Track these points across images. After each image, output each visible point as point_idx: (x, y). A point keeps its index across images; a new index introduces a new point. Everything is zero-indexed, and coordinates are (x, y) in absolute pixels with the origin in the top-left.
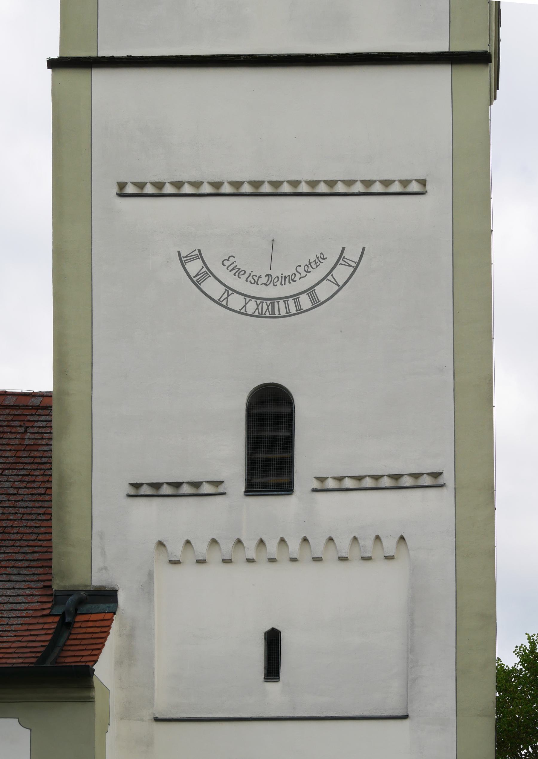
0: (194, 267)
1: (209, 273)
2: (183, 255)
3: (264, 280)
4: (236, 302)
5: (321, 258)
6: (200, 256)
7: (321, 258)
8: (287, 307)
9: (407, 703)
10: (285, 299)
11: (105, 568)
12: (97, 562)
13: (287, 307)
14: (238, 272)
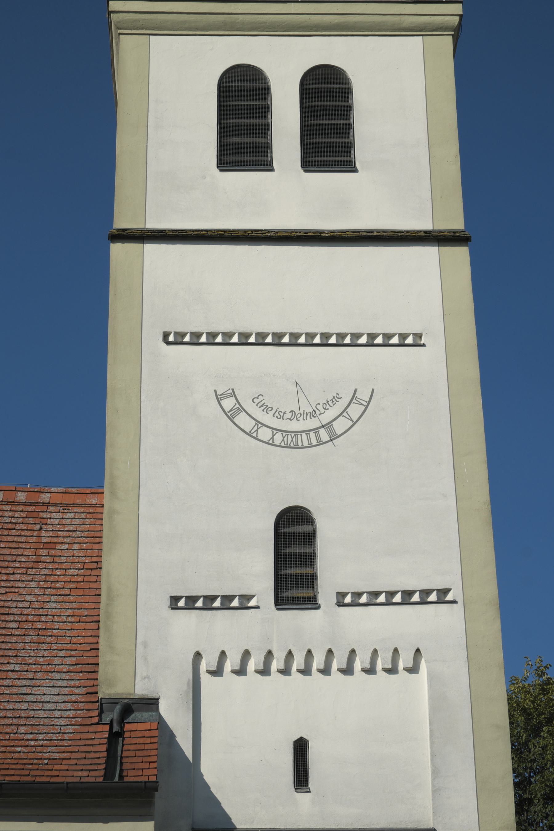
0: (229, 403)
1: (241, 409)
2: (219, 393)
3: (288, 415)
4: (265, 434)
5: (337, 398)
6: (233, 394)
7: (337, 398)
8: (309, 439)
9: (436, 791)
10: (307, 432)
11: (148, 677)
12: (141, 671)
13: (309, 439)
14: (266, 409)
